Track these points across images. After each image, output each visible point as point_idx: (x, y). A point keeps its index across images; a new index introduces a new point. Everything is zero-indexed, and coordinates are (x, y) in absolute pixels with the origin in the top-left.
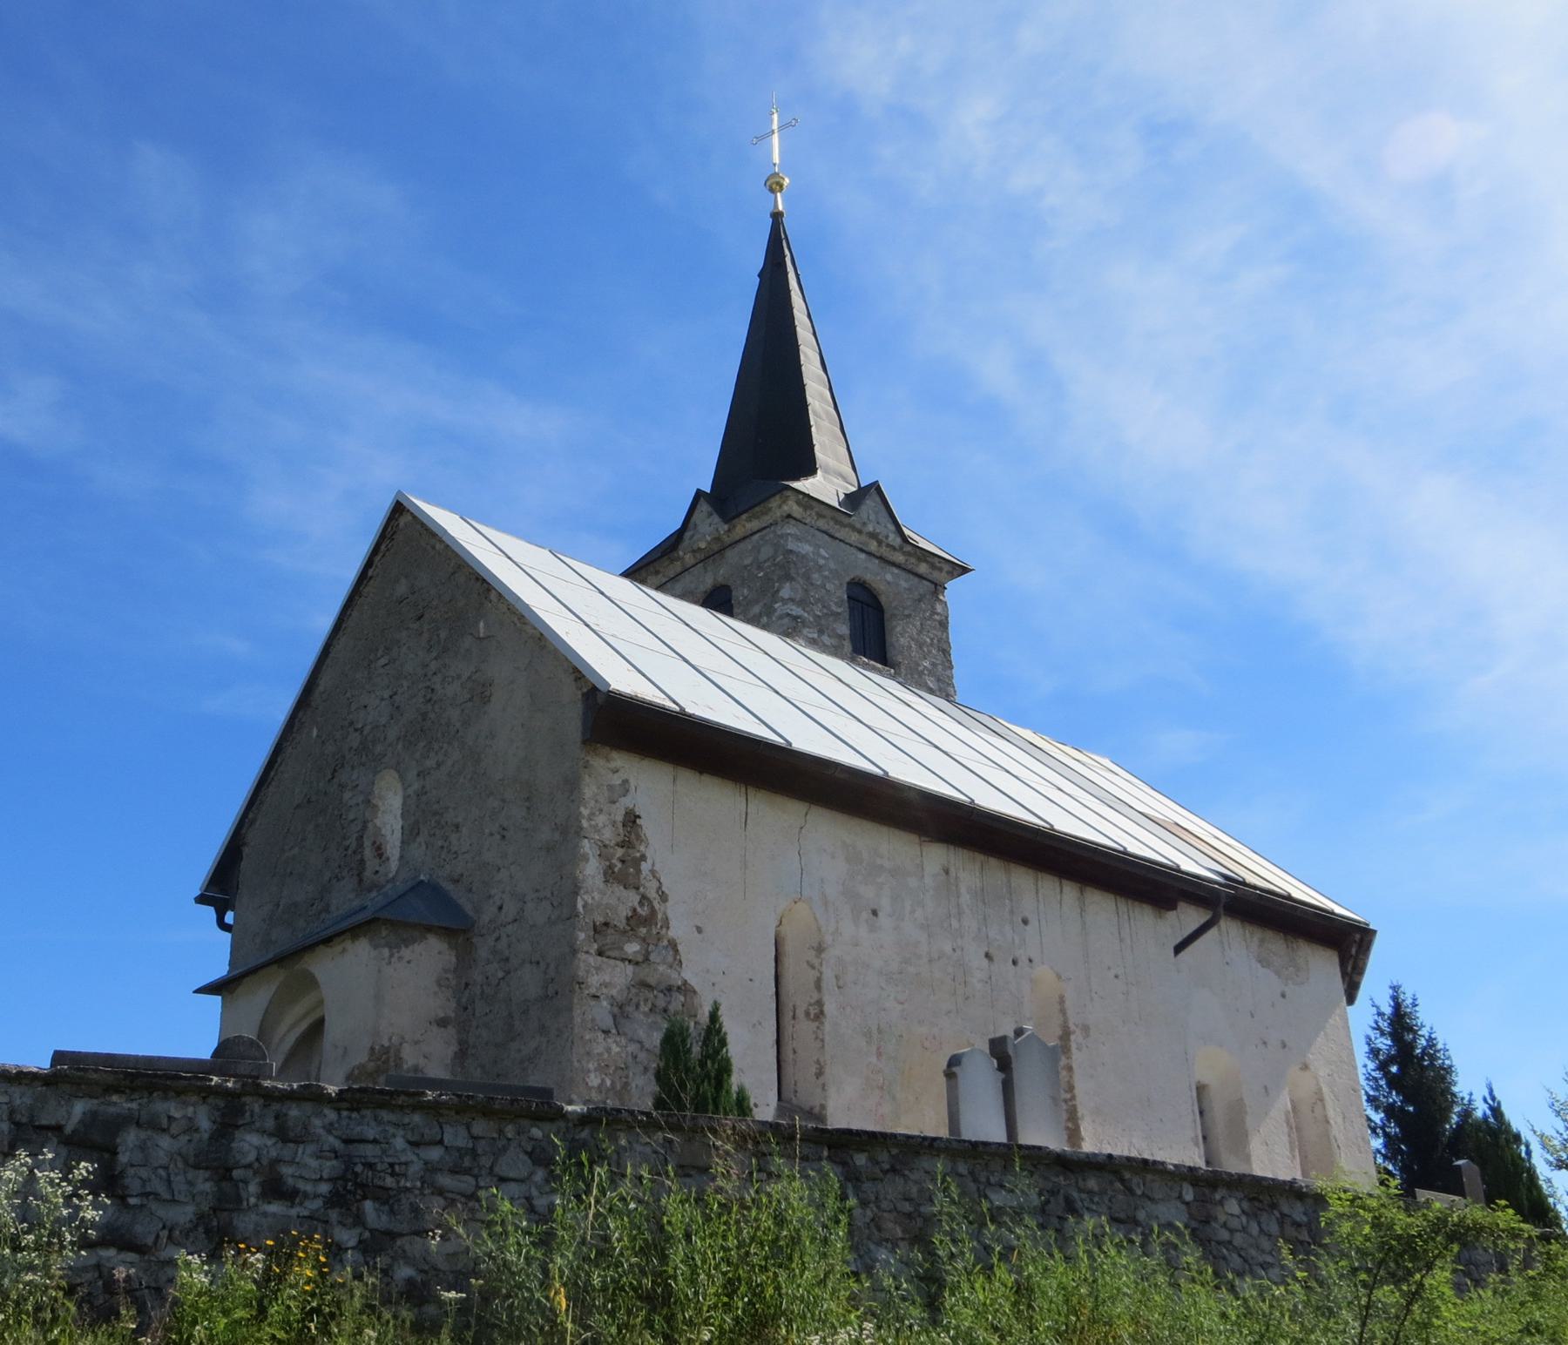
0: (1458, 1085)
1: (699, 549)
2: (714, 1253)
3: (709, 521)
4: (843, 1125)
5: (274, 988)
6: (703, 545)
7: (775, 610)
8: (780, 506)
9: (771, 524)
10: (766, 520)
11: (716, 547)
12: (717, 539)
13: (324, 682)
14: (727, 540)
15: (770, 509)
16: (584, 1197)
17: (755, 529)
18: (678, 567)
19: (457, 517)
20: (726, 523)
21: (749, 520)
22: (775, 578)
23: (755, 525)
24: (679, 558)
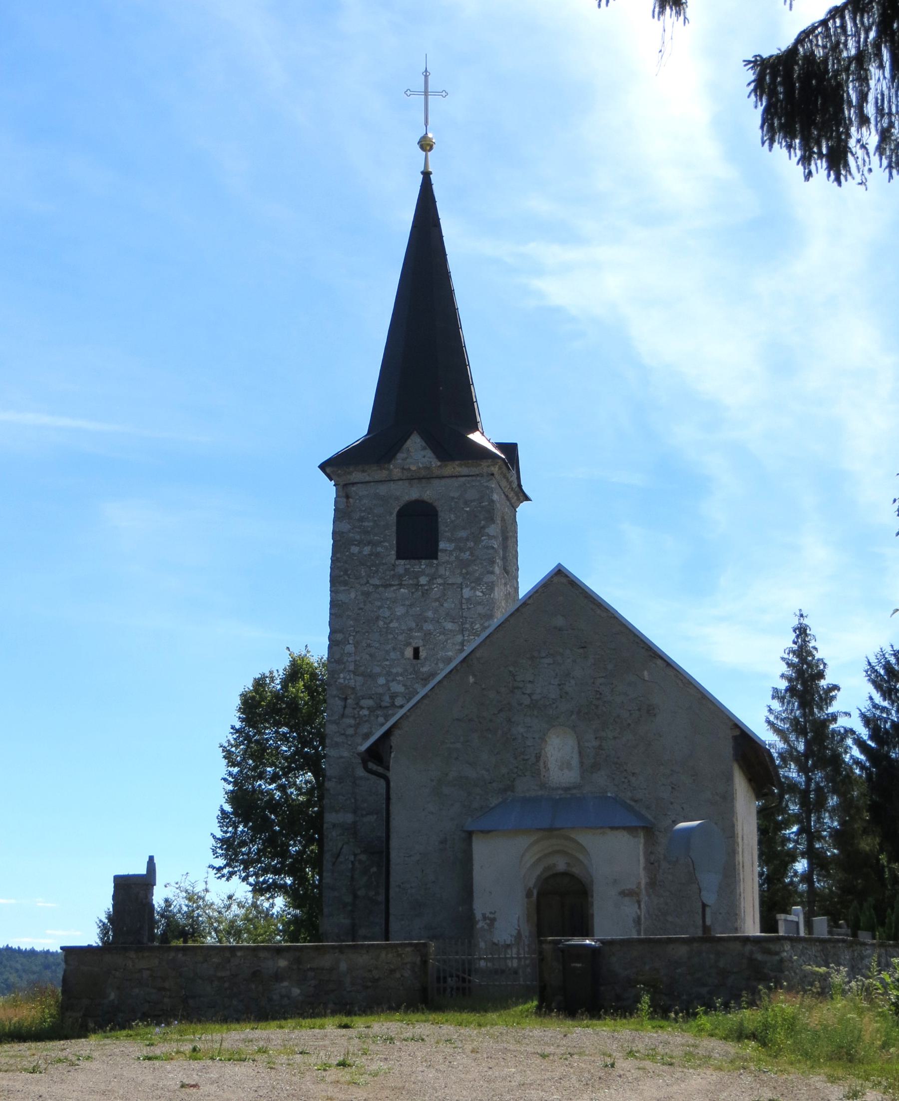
0: (828, 673)
1: (409, 469)
2: (6, 1051)
3: (423, 453)
4: (146, 870)
5: (536, 838)
6: (413, 468)
7: (483, 541)
8: (488, 466)
9: (478, 475)
10: (474, 471)
11: (423, 473)
12: (427, 468)
13: (659, 662)
14: (437, 472)
15: (481, 465)
16: (108, 1028)
17: (463, 474)
18: (383, 474)
19: (521, 504)
20: (440, 461)
21: (460, 466)
22: (482, 517)
23: (464, 470)
24: (388, 469)
